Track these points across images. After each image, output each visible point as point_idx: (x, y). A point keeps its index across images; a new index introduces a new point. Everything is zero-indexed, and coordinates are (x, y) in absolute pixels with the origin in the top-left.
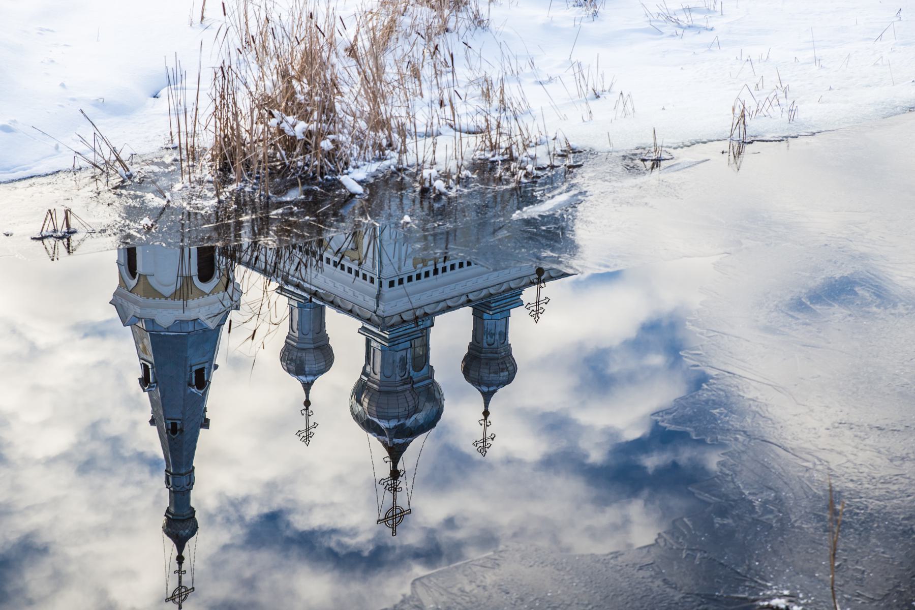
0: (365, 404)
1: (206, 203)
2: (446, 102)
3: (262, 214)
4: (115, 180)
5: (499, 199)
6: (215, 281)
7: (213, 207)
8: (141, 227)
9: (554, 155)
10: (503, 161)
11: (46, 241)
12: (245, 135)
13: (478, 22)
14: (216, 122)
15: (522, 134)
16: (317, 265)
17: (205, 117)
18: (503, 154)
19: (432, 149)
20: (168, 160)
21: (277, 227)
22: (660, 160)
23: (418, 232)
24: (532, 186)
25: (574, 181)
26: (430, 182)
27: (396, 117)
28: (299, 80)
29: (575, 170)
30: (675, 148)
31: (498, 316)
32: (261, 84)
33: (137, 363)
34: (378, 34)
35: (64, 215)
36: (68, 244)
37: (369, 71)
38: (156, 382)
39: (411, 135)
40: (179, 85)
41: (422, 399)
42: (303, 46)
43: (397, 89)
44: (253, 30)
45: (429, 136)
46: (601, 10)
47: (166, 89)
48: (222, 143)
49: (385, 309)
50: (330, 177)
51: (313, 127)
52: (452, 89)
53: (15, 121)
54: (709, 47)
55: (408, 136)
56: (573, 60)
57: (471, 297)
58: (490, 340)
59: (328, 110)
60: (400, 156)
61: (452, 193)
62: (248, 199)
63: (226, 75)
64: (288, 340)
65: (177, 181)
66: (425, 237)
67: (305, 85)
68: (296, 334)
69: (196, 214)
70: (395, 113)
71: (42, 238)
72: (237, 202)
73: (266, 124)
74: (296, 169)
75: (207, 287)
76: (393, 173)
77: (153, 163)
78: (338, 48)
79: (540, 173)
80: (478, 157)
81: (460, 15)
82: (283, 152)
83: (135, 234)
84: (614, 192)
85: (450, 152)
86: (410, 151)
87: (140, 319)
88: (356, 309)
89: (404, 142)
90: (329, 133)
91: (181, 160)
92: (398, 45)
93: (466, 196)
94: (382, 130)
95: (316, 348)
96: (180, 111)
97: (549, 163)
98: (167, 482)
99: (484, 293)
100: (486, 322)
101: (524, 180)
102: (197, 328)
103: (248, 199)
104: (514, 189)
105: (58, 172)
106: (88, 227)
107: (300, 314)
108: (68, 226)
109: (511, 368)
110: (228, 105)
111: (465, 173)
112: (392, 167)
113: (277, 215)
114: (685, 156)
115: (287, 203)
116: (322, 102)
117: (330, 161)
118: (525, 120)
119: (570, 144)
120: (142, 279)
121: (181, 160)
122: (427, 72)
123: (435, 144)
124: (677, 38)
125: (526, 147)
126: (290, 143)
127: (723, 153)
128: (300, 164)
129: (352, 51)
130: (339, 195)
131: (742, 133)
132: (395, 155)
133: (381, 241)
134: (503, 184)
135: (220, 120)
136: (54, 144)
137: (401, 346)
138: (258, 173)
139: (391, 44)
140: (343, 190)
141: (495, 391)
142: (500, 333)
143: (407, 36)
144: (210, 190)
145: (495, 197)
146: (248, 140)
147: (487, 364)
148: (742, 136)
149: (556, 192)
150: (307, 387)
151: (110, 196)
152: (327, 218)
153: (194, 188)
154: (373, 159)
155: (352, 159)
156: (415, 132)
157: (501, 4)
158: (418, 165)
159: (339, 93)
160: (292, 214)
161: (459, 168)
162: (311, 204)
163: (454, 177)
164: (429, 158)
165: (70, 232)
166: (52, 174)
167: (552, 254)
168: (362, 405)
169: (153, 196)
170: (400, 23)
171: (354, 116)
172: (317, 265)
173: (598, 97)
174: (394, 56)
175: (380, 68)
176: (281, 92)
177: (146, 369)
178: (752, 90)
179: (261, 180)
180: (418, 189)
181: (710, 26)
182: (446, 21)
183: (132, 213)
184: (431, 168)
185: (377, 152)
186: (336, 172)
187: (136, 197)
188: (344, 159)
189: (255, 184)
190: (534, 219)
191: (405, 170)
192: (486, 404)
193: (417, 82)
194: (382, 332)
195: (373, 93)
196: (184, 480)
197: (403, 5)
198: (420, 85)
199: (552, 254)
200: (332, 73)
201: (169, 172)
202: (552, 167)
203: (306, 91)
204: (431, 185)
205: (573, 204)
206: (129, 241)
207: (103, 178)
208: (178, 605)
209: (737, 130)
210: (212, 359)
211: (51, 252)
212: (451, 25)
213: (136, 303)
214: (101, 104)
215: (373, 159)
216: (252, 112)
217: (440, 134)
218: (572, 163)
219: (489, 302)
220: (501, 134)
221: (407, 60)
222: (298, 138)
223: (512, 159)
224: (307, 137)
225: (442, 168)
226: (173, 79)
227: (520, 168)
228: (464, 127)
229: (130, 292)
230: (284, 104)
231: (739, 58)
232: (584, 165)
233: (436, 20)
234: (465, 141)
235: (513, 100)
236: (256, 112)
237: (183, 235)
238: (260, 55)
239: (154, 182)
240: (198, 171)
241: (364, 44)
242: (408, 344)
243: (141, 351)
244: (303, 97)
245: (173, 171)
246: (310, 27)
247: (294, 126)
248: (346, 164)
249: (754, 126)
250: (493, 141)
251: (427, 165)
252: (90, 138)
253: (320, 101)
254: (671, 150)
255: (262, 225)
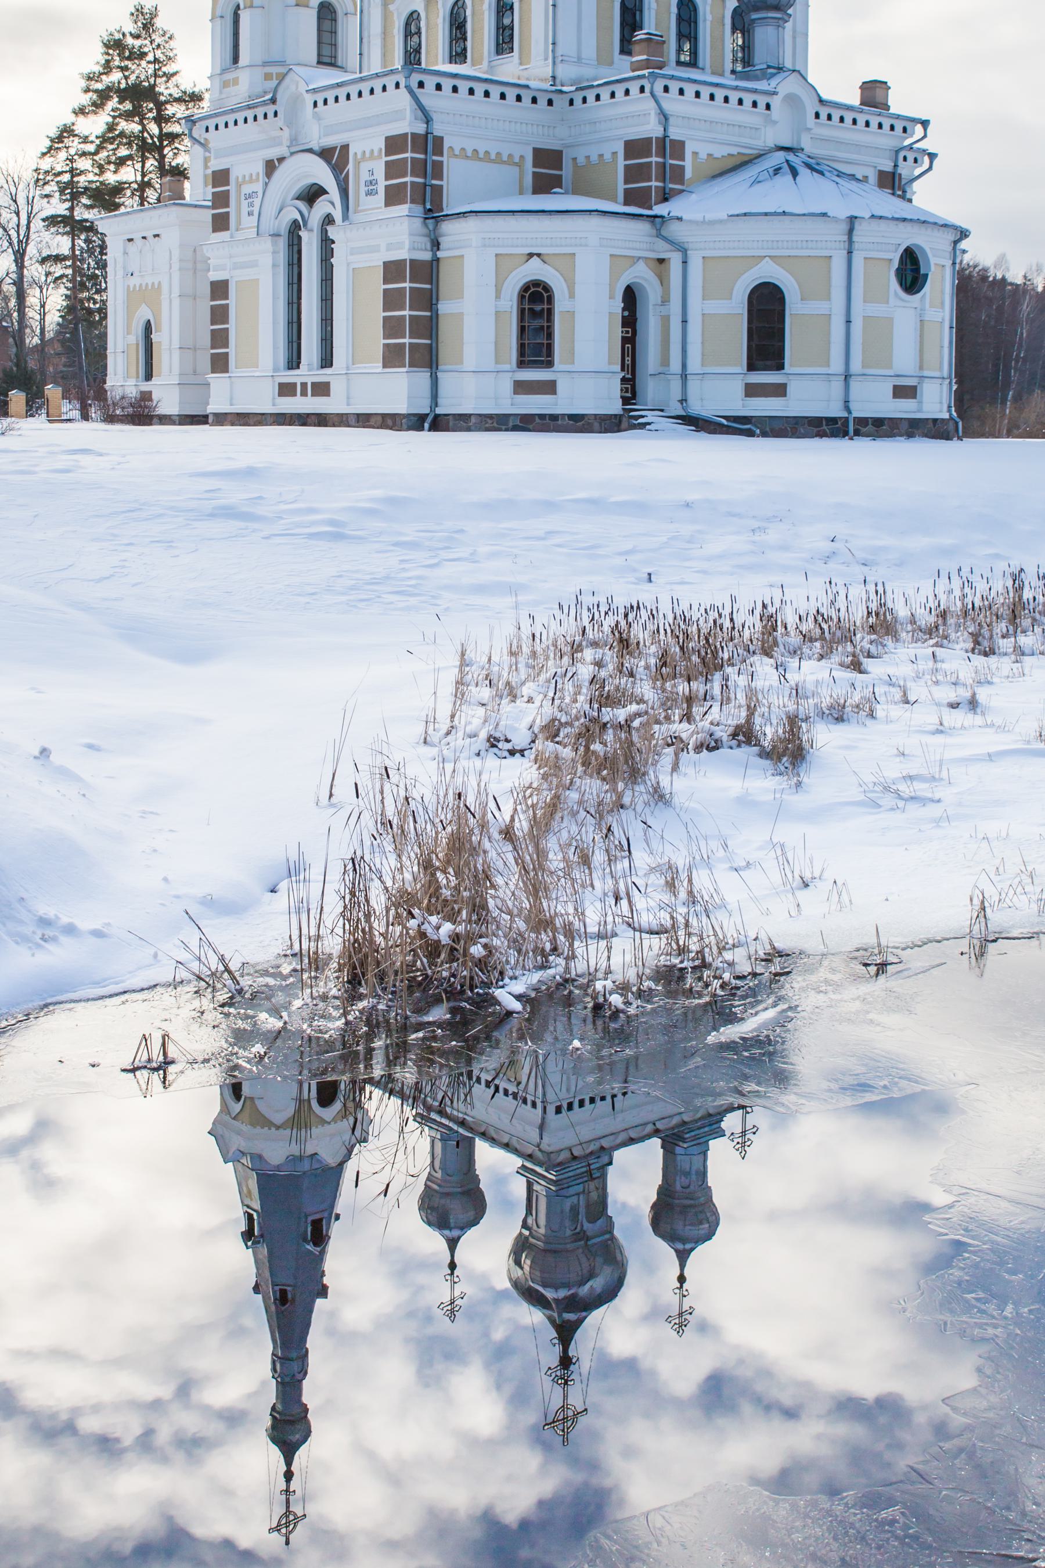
0: (527, 1268)
1: (330, 1025)
2: (623, 894)
3: (398, 1038)
4: (223, 996)
5: (690, 1017)
6: (338, 1105)
7: (338, 1029)
8: (252, 1056)
9: (756, 959)
10: (694, 968)
11: (138, 1073)
12: (379, 940)
13: (659, 796)
14: (344, 924)
15: (716, 935)
16: (466, 1099)
17: (333, 916)
18: (693, 960)
19: (606, 954)
20: (286, 969)
21: (416, 1055)
22: (886, 965)
23: (590, 1060)
24: (730, 1000)
25: (783, 992)
26: (604, 995)
27: (562, 915)
28: (445, 872)
29: (782, 978)
30: (903, 949)
31: (695, 1150)
32: (398, 877)
33: (239, 1213)
34: (539, 813)
35: (161, 1041)
36: (165, 1078)
37: (528, 857)
38: (262, 1236)
39: (580, 937)
40: (302, 877)
41: (599, 1260)
42: (449, 829)
43: (563, 880)
44: (390, 812)
45: (602, 938)
46: (806, 780)
47: (286, 881)
48: (352, 950)
49: (550, 1142)
50: (481, 991)
51: (461, 929)
52: (629, 878)
53: (109, 924)
54: (937, 822)
55: (577, 937)
56: (775, 841)
57: (660, 1125)
58: (685, 1181)
59: (479, 908)
60: (567, 964)
61: (632, 1010)
62: (381, 1019)
63: (357, 867)
64: (429, 1183)
65: (297, 997)
66: (600, 1068)
67: (451, 878)
68: (439, 1175)
69: (319, 1038)
70: (560, 909)
71: (133, 1070)
72: (368, 1023)
73: (404, 927)
74: (441, 980)
75: (328, 1113)
76: (559, 984)
77: (266, 973)
78: (491, 830)
79: (739, 983)
80: (662, 963)
81: (637, 788)
82: (425, 960)
83: (244, 1064)
84: (831, 1007)
85: (629, 957)
86: (581, 959)
87: (243, 1154)
88: (514, 1142)
89: (571, 945)
90: (481, 937)
91: (302, 970)
92: (564, 825)
93: (649, 1013)
94: (545, 931)
95: (463, 1193)
96: (301, 908)
97: (750, 970)
98: (274, 1370)
99: (675, 1121)
100: (679, 1158)
101: (720, 992)
102: (315, 1166)
103: (381, 1019)
104: (707, 1004)
105: (155, 986)
106: (189, 1056)
107: (444, 1149)
108: (165, 1054)
109: (712, 1219)
110: (359, 903)
111: (647, 984)
112: (558, 977)
113: (416, 1039)
114: (916, 960)
115: (429, 1023)
116: (472, 898)
117: (481, 970)
118: (720, 917)
119: (776, 945)
120: (248, 1103)
121: (302, 970)
122: (599, 858)
123: (609, 949)
124: (898, 811)
125: (721, 949)
126: (433, 949)
127: (962, 954)
128: (445, 974)
129: (508, 833)
130: (493, 1013)
131: (983, 929)
132: (561, 961)
133: (544, 1069)
134: (694, 998)
135: (349, 921)
136: (152, 951)
137: (572, 1191)
138: (394, 986)
139: (555, 825)
140: (498, 1008)
141: (693, 1249)
142: (697, 1173)
143: (574, 814)
144: (336, 1008)
145: (685, 1014)
146: (383, 945)
147: (681, 1213)
148: (983, 932)
149: (760, 1007)
150: (452, 1244)
151: (213, 1016)
152: (478, 1043)
153: (316, 1005)
154: (534, 967)
155: (508, 967)
156: (585, 932)
157: (685, 774)
158: (590, 974)
159: (493, 886)
160: (435, 1038)
161: (640, 977)
162: (458, 1024)
163: (634, 989)
164: (603, 964)
165: (168, 1062)
166: (147, 989)
167: (757, 1088)
168: (522, 1268)
169: (267, 1016)
170: (565, 798)
171: (510, 913)
172: (466, 1099)
173: (807, 885)
174: (559, 840)
175: (541, 854)
176: (423, 886)
177: (250, 1218)
178: (992, 876)
179: (398, 995)
180: (590, 1005)
181: (937, 797)
182: (620, 796)
183: (241, 1037)
184: (606, 979)
185: (539, 958)
186: (488, 985)
187: (247, 1017)
188: (499, 967)
189: (390, 1000)
190: (734, 1042)
191: (574, 980)
192: (682, 1266)
193: (587, 871)
194: (547, 1171)
195: (534, 886)
196: (295, 1366)
197: (569, 777)
198: (591, 874)
199: (757, 1088)
200: (484, 861)
201: (287, 985)
202: (755, 975)
203: (453, 884)
204: (605, 1000)
205: (782, 1022)
206: (237, 1073)
207: (208, 993)
208: (284, 1538)
209: (977, 926)
210: (332, 1206)
211: (144, 1087)
212: (626, 800)
213: (239, 1133)
214: (209, 902)
215: (534, 967)
216: (387, 912)
217: (616, 935)
218: (778, 970)
219: (682, 1132)
220: (690, 935)
221: (574, 844)
222: (443, 943)
223: (705, 965)
224: (454, 941)
225: (619, 978)
226: (295, 870)
227: (715, 977)
228: (645, 925)
229: (234, 1118)
230: (426, 902)
231: (973, 835)
232: (794, 972)
233: (609, 795)
234: (646, 944)
235: (704, 892)
236: (392, 912)
237: (301, 1065)
238: (398, 840)
239: (268, 998)
240: (322, 984)
241: (522, 825)
242: (580, 1188)
243: (244, 1194)
244: (449, 893)
245: (292, 984)
246: (458, 807)
247: (438, 928)
248: (501, 973)
249: (997, 919)
250: (681, 943)
251: (600, 975)
252: (194, 944)
253: (470, 898)
254: (899, 952)
255: (397, 1053)
